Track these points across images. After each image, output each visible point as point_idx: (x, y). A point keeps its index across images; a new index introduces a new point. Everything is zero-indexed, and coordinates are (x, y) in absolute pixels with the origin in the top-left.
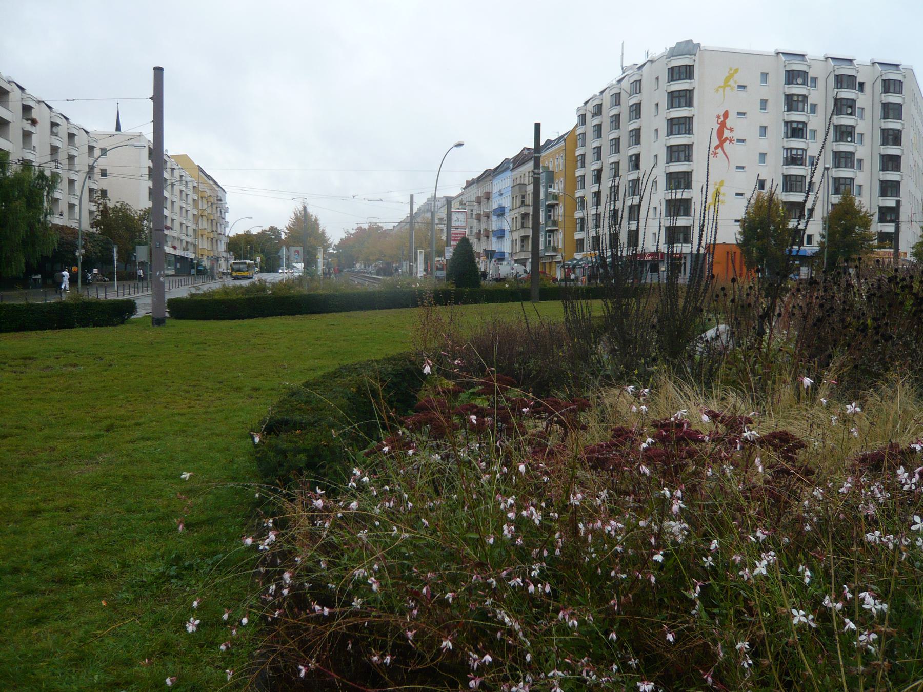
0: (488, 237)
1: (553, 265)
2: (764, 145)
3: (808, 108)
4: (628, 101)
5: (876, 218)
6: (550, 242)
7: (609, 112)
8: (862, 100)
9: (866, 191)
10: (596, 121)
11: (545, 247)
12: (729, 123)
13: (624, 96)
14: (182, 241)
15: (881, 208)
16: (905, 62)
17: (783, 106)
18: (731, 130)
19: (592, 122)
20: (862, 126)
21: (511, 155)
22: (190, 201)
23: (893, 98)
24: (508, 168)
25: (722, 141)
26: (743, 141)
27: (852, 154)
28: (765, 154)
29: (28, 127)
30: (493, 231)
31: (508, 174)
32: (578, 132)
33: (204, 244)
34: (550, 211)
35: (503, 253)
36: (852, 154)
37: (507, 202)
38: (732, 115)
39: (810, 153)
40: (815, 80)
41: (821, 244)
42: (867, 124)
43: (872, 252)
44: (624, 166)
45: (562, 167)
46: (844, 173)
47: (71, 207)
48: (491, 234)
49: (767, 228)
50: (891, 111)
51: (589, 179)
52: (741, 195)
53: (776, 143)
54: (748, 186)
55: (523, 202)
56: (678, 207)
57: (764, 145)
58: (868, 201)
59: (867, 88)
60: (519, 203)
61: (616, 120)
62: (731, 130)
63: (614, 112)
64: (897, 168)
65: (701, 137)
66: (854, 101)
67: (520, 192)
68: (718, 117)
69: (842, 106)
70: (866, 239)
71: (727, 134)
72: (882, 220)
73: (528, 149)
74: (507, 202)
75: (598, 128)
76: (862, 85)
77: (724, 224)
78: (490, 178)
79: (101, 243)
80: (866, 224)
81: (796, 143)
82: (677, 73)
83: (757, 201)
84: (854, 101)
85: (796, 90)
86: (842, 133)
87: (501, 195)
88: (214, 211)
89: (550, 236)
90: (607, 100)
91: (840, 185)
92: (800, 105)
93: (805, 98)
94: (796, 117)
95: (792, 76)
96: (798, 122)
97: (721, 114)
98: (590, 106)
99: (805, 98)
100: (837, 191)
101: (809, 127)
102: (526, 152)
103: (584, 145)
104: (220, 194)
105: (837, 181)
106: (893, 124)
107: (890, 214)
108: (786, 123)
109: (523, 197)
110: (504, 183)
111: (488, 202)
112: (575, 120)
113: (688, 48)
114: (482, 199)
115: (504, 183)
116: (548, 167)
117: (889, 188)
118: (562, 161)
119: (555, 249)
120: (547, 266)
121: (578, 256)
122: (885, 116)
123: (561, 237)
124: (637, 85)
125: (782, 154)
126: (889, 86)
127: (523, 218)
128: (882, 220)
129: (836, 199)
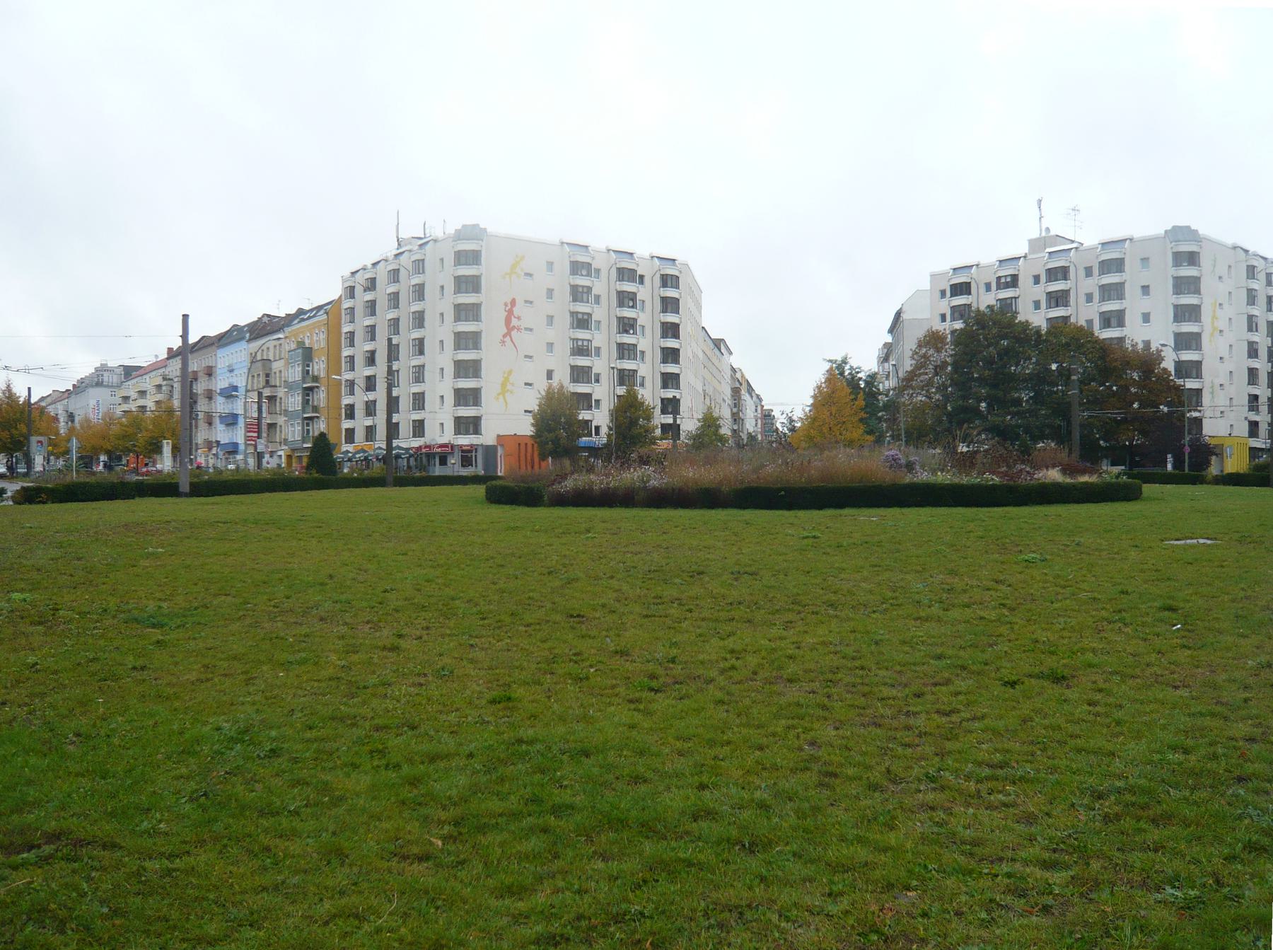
0: (210, 424)
2: (551, 334)
3: (592, 299)
4: (408, 281)
5: (658, 411)
7: (385, 288)
8: (643, 293)
9: (648, 383)
10: (369, 296)
12: (516, 311)
13: (403, 273)
15: (662, 400)
16: (680, 258)
17: (568, 297)
18: (519, 318)
19: (363, 297)
20: (643, 318)
21: (243, 321)
23: (671, 293)
24: (242, 339)
25: (510, 328)
26: (531, 330)
27: (635, 346)
28: (552, 344)
31: (243, 344)
35: (236, 445)
36: (635, 346)
37: (241, 381)
38: (519, 303)
39: (595, 344)
40: (598, 271)
41: (609, 436)
42: (648, 317)
43: (655, 444)
44: (359, 312)
45: (323, 344)
46: (628, 365)
48: (217, 421)
49: (558, 428)
50: (670, 305)
51: (359, 361)
52: (530, 385)
53: (563, 334)
54: (542, 385)
55: (267, 382)
56: (467, 397)
57: (551, 334)
58: (650, 394)
59: (647, 280)
61: (394, 299)
62: (519, 318)
63: (391, 289)
64: (676, 335)
65: (490, 325)
66: (635, 294)
68: (506, 305)
69: (626, 299)
70: (649, 431)
71: (514, 322)
72: (664, 411)
74: (241, 381)
75: (372, 307)
76: (642, 277)
77: (508, 416)
80: (649, 418)
81: (582, 334)
82: (463, 258)
83: (548, 392)
84: (635, 294)
85: (582, 281)
86: (624, 325)
87: (231, 371)
90: (382, 275)
91: (625, 377)
92: (585, 296)
93: (589, 289)
94: (582, 308)
95: (576, 267)
96: (583, 314)
97: (509, 301)
98: (361, 278)
99: (589, 289)
100: (621, 383)
101: (594, 318)
102: (266, 319)
105: (621, 371)
106: (671, 318)
107: (671, 406)
108: (573, 314)
109: (267, 375)
111: (210, 380)
113: (472, 232)
114: (200, 374)
117: (670, 380)
118: (323, 337)
122: (664, 310)
124: (419, 266)
125: (569, 345)
126: (668, 281)
128: (664, 411)
129: (621, 391)
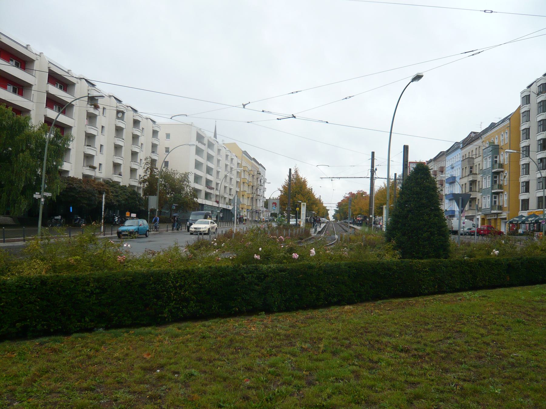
1: (498, 221)
6: (495, 202)
11: (492, 206)
14: (225, 198)
22: (235, 172)
29: (92, 110)
30: (446, 195)
31: (459, 151)
32: (523, 110)
33: (246, 202)
34: (496, 177)
37: (457, 173)
45: (507, 141)
47: (217, 184)
55: (471, 172)
60: (468, 171)
67: (469, 164)
73: (474, 133)
74: (457, 173)
78: (444, 156)
79: (128, 194)
87: (453, 168)
88: (255, 180)
89: (495, 198)
102: (473, 135)
103: (528, 120)
104: (261, 170)
109: (471, 168)
110: (456, 158)
112: (518, 102)
114: (438, 172)
115: (456, 158)
116: (494, 143)
118: (506, 136)
119: (500, 208)
120: (493, 222)
121: (525, 214)
123: (505, 198)
127: (471, 184)
